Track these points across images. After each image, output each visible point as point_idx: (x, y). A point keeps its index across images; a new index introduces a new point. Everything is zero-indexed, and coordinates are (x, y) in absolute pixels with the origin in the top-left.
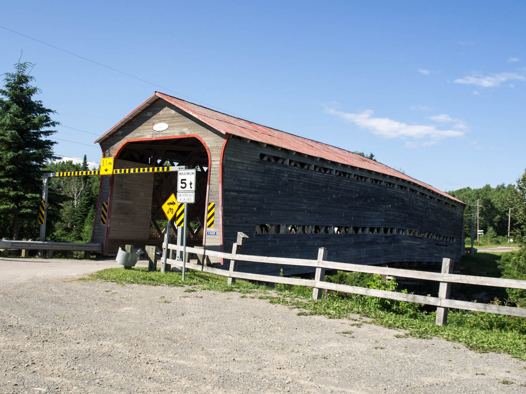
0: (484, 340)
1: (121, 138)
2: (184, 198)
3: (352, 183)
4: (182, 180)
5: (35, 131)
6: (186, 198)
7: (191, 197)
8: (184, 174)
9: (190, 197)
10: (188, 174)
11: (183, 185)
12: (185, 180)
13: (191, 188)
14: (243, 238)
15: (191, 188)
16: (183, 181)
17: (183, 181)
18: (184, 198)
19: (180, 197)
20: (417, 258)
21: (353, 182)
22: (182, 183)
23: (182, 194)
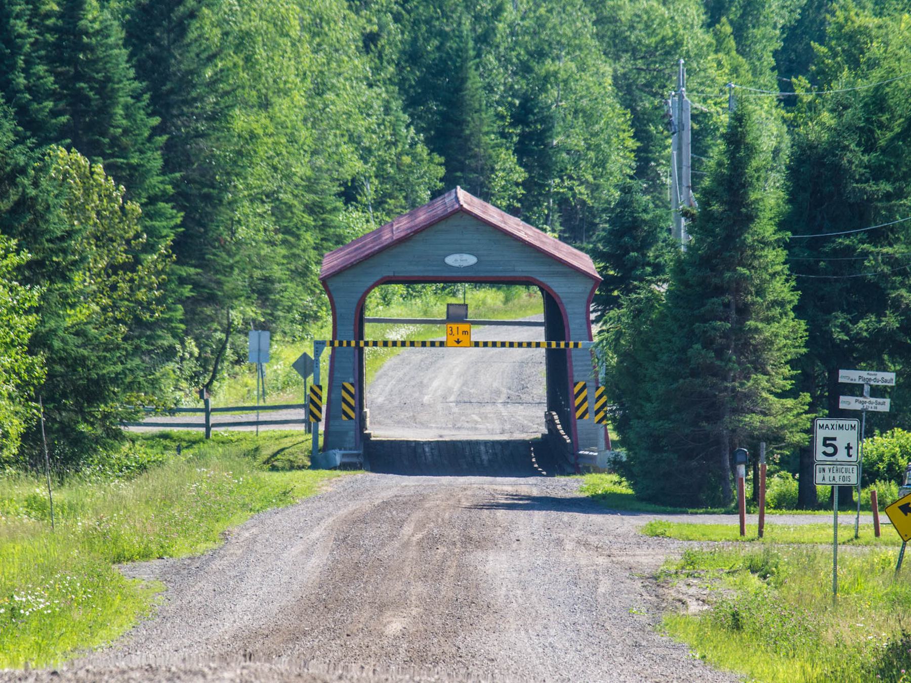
0: (116, 207)
1: (569, 470)
2: (832, 475)
3: (165, 436)
4: (825, 439)
5: (587, 453)
6: (837, 475)
7: (851, 475)
8: (830, 427)
9: (848, 474)
10: (841, 427)
11: (830, 450)
12: (834, 439)
13: (849, 455)
14: (305, 355)
15: (849, 455)
16: (828, 442)
17: (828, 442)
18: (832, 475)
19: (822, 474)
20: (336, 365)
21: (175, 430)
22: (825, 445)
23: (827, 467)
